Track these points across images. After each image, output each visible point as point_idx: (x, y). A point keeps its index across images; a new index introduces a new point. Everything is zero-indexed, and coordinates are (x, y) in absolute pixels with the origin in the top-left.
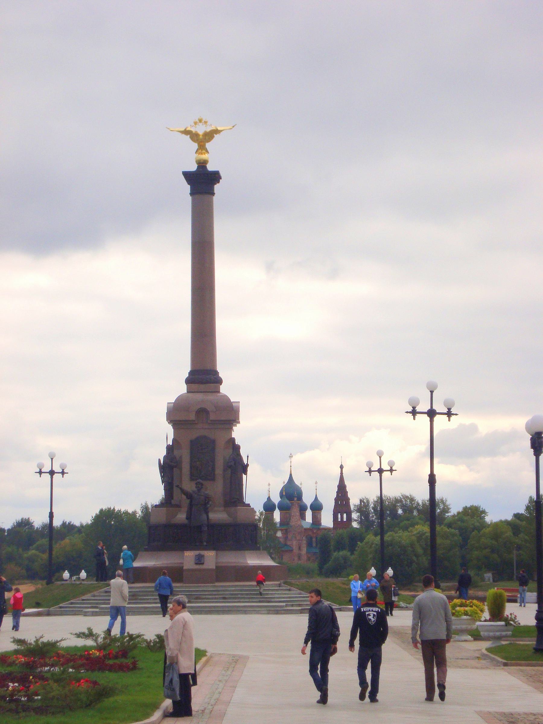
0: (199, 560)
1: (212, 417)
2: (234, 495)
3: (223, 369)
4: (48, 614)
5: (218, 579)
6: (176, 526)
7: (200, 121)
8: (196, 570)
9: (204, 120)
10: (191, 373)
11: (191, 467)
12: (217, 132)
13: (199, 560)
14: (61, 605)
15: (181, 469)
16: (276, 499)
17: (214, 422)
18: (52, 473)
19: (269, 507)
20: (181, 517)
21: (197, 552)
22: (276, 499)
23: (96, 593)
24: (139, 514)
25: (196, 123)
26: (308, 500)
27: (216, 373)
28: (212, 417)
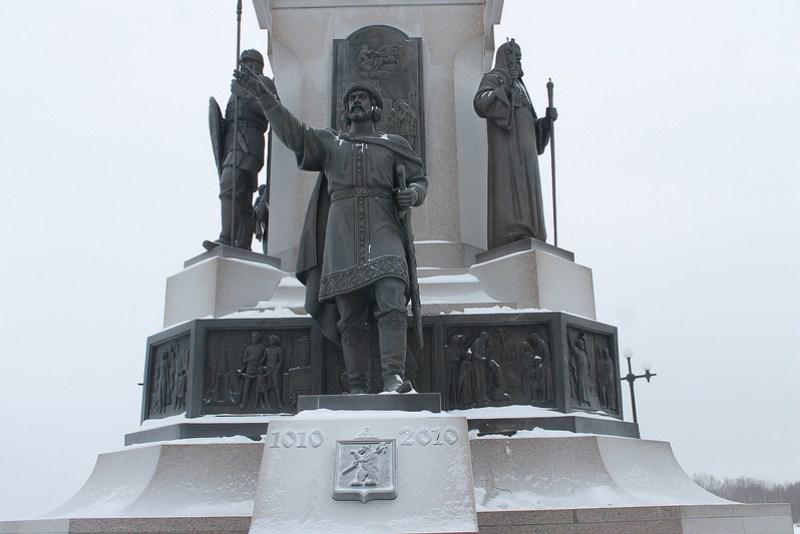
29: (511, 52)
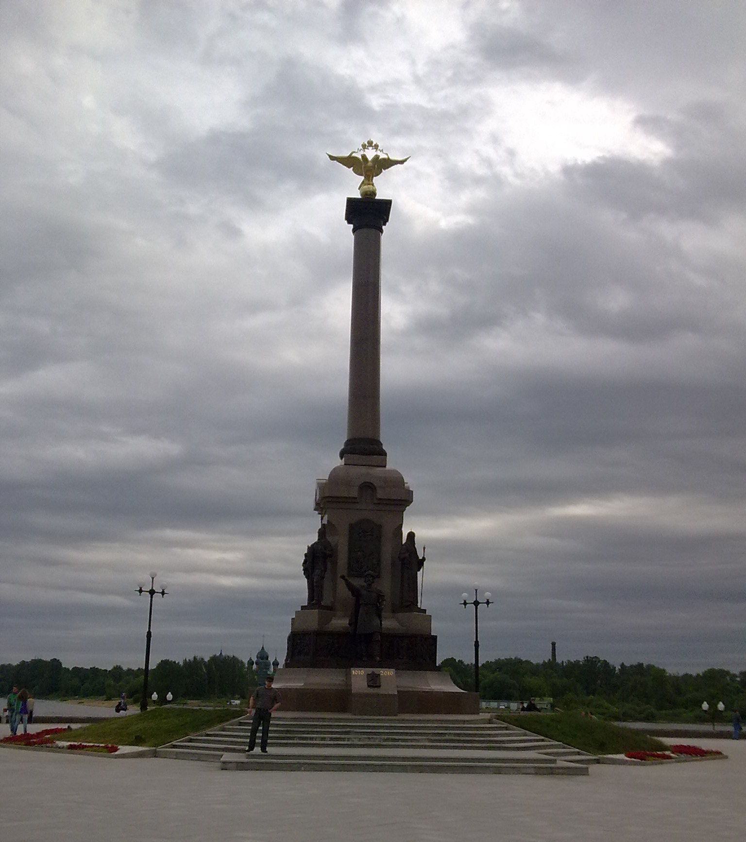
0: (374, 681)
1: (380, 494)
2: (407, 595)
3: (387, 438)
4: (155, 755)
5: (403, 709)
6: (332, 634)
7: (370, 143)
8: (367, 695)
9: (374, 143)
10: (347, 443)
11: (350, 558)
12: (388, 163)
13: (374, 681)
14: (174, 743)
15: (335, 563)
16: (255, 659)
17: (380, 502)
18: (152, 592)
19: (251, 663)
20: (340, 623)
21: (370, 670)
22: (255, 659)
23: (226, 725)
24: (181, 663)
25: (364, 147)
26: (271, 660)
27: (379, 444)
28: (380, 494)
29: (411, 536)
